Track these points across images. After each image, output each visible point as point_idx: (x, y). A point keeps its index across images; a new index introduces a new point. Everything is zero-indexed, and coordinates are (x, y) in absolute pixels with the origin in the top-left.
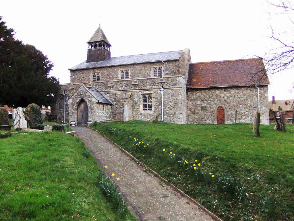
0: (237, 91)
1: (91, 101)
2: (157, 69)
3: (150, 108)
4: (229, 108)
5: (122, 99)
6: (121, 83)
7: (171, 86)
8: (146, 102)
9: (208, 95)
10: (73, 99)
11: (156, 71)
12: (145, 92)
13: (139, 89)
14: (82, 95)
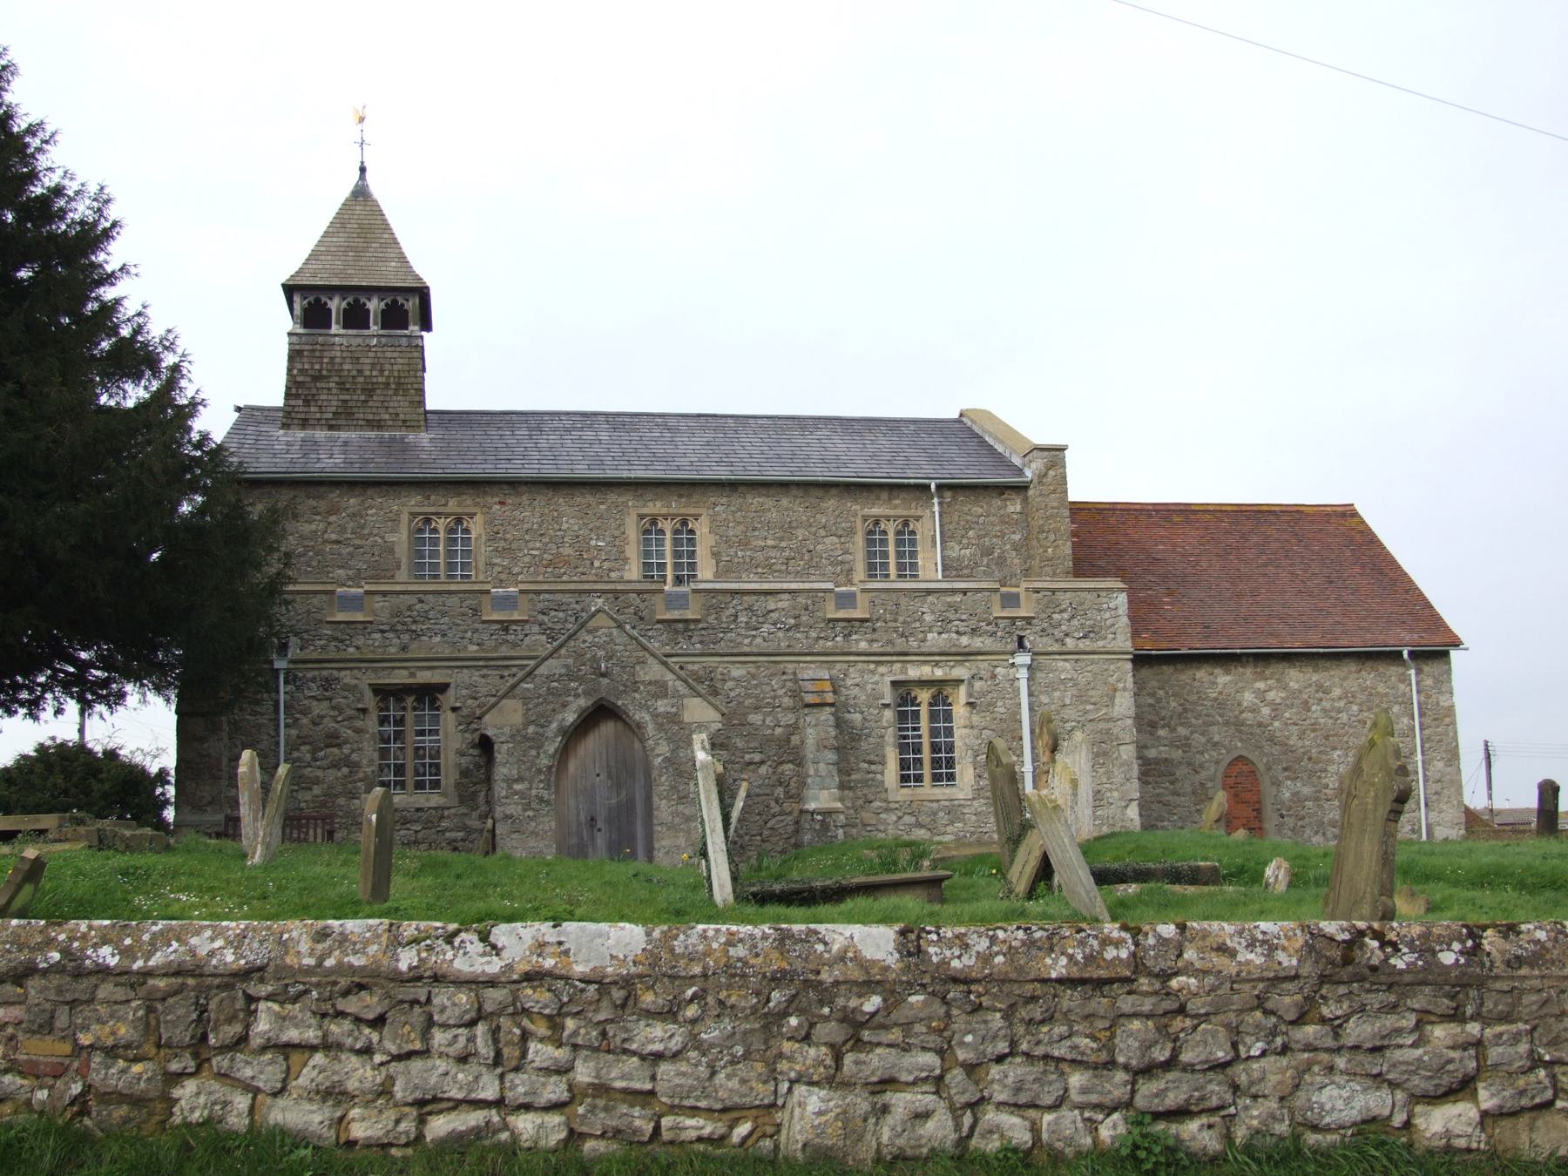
0: (1315, 677)
1: (674, 718)
2: (891, 528)
3: (944, 771)
4: (1285, 769)
5: (757, 708)
6: (750, 609)
7: (1068, 640)
8: (905, 737)
9: (1175, 695)
10: (525, 699)
11: (884, 542)
12: (914, 673)
13: (876, 647)
14: (603, 675)
